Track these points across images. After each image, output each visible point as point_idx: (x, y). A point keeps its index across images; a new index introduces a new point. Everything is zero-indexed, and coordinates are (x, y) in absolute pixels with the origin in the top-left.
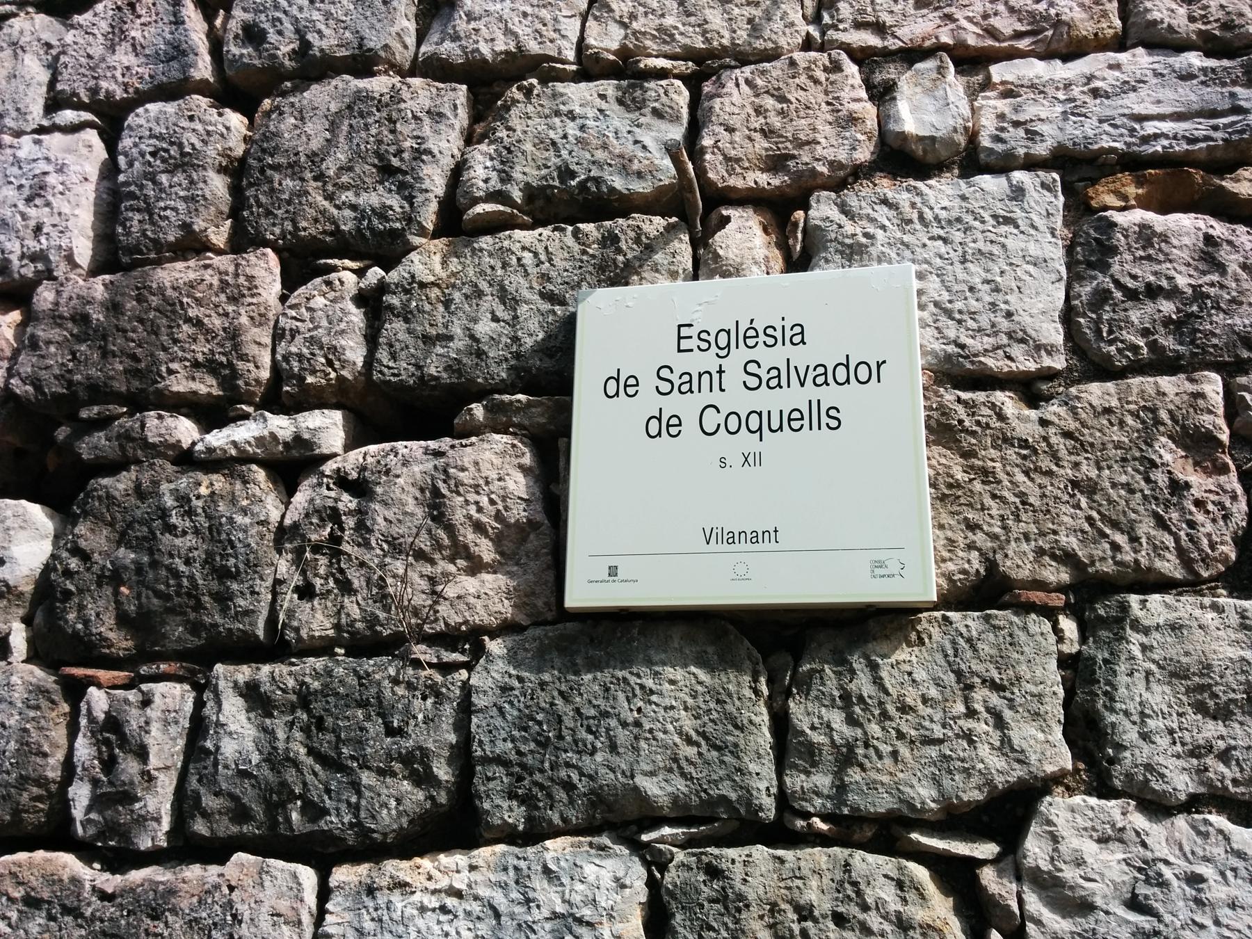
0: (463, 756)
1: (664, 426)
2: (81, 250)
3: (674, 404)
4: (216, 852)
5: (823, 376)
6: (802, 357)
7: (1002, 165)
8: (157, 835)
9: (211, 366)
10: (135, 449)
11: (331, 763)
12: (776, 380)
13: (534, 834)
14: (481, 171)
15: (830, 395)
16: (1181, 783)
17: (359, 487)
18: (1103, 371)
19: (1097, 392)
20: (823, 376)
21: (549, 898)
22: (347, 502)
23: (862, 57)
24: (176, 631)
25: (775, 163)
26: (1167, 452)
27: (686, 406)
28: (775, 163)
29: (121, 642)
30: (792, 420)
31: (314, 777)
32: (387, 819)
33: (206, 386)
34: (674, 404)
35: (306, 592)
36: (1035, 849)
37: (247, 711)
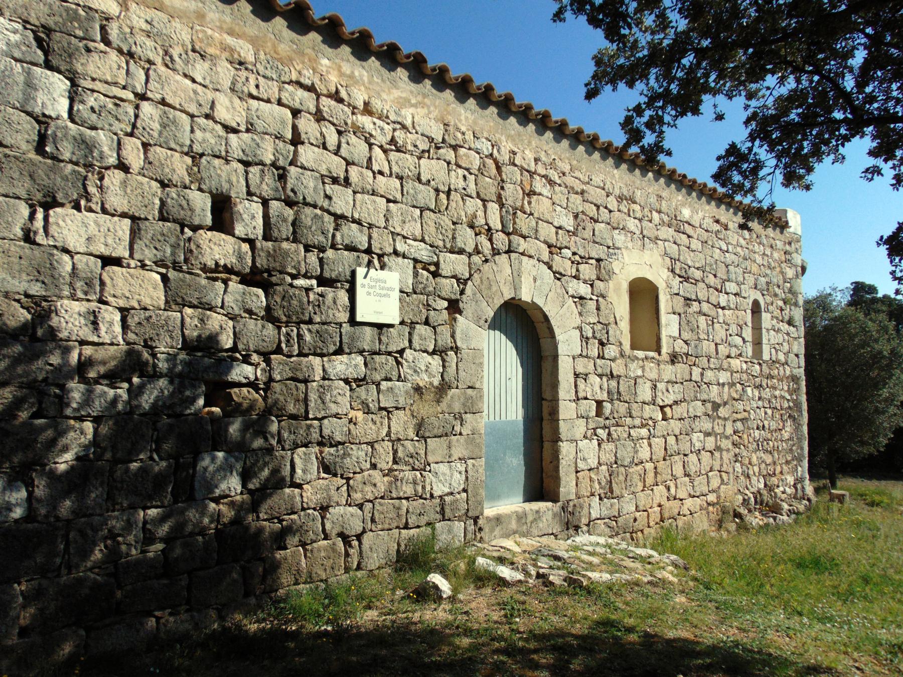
0: (341, 341)
1: (369, 294)
2: (565, 365)
3: (370, 290)
4: (306, 355)
5: (388, 289)
6: (386, 286)
7: (408, 258)
8: (296, 353)
9: (294, 267)
10: (668, 558)
11: (324, 342)
12: (383, 289)
13: (349, 354)
14: (338, 238)
15: (389, 292)
16: (418, 348)
17: (322, 295)
18: (415, 293)
19: (415, 296)
20: (388, 289)
21: (354, 363)
22: (321, 299)
23: (392, 233)
24: (294, 318)
25: (381, 249)
26: (421, 306)
27: (371, 291)
28: (381, 249)
29: (284, 319)
30: (385, 295)
31: (320, 344)
32: (331, 351)
33: (294, 272)
34: (370, 290)
35: (315, 313)
36: (405, 356)
37: (647, 635)
